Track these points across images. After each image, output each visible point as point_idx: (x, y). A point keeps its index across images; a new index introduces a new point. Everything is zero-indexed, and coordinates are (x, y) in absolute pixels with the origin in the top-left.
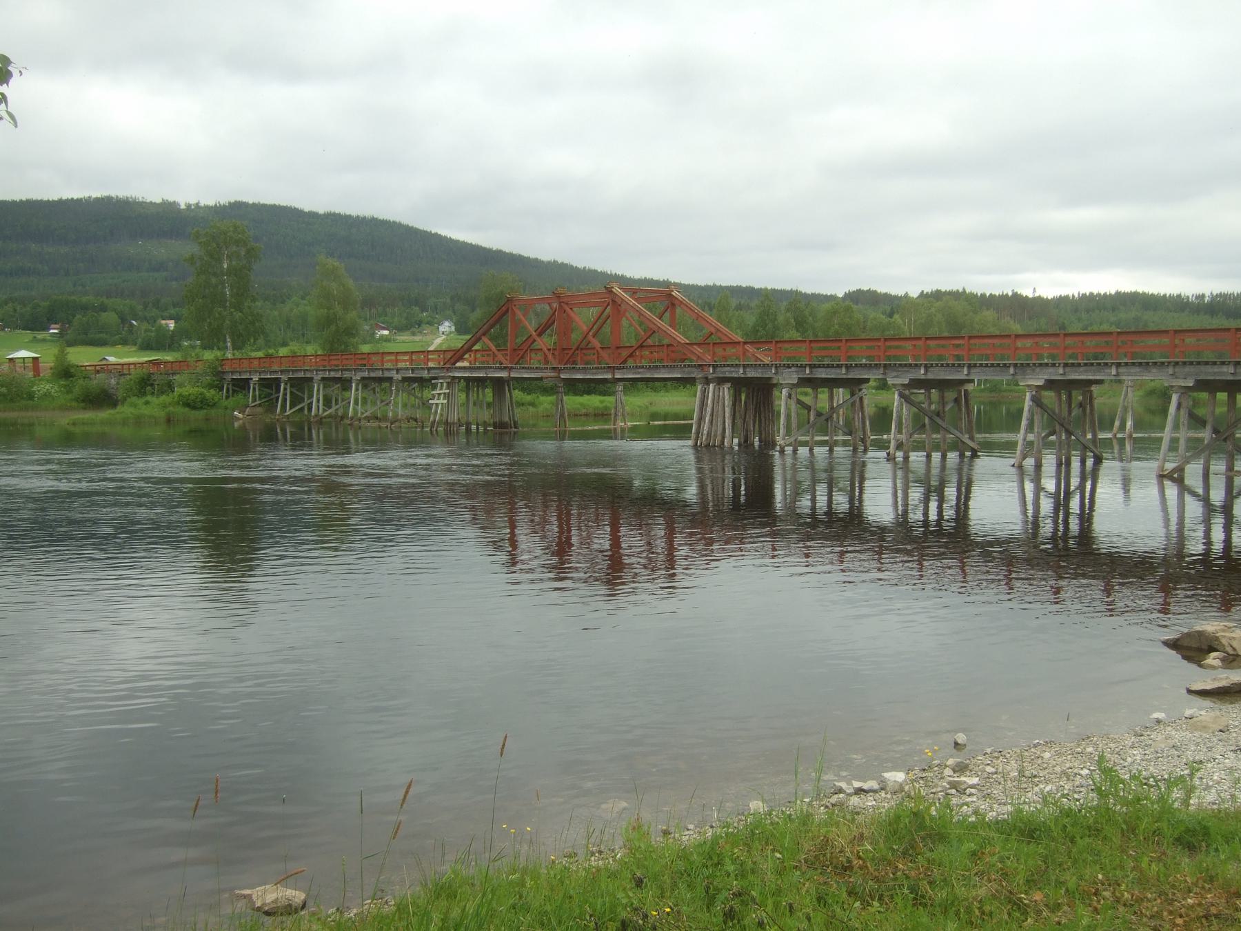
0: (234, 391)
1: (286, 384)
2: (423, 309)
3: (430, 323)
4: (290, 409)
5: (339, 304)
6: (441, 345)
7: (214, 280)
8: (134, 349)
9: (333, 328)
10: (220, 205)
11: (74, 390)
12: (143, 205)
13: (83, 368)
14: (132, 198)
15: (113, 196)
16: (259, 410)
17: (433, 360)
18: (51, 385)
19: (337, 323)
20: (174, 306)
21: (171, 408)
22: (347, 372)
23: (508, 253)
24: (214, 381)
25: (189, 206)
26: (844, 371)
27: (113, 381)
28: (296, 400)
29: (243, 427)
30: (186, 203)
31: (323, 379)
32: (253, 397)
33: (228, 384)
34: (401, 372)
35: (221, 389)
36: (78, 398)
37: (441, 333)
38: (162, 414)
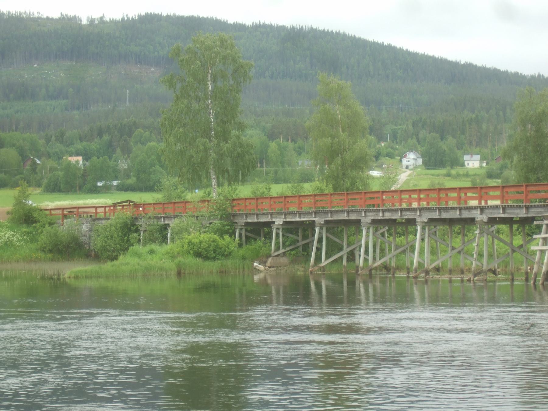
0: (247, 238)
1: (321, 228)
2: (381, 138)
3: (390, 155)
4: (327, 257)
5: (343, 131)
6: (407, 182)
7: (195, 106)
8: (38, 191)
9: (338, 160)
10: (128, 19)
11: (39, 239)
12: (38, 21)
13: (48, 212)
14: (25, 13)
15: (5, 12)
16: (284, 260)
17: (453, 199)
18: (12, 233)
19: (342, 155)
20: (81, 140)
21: (181, 259)
22: (408, 213)
23: (479, 68)
24: (224, 226)
25: (92, 21)
26: (524, 211)
27: (85, 228)
28: (333, 248)
29: (264, 282)
30: (88, 18)
31: (374, 222)
32: (275, 245)
33: (241, 229)
34: (487, 211)
35: (234, 233)
36: (45, 248)
37: (404, 167)
38: (171, 265)
